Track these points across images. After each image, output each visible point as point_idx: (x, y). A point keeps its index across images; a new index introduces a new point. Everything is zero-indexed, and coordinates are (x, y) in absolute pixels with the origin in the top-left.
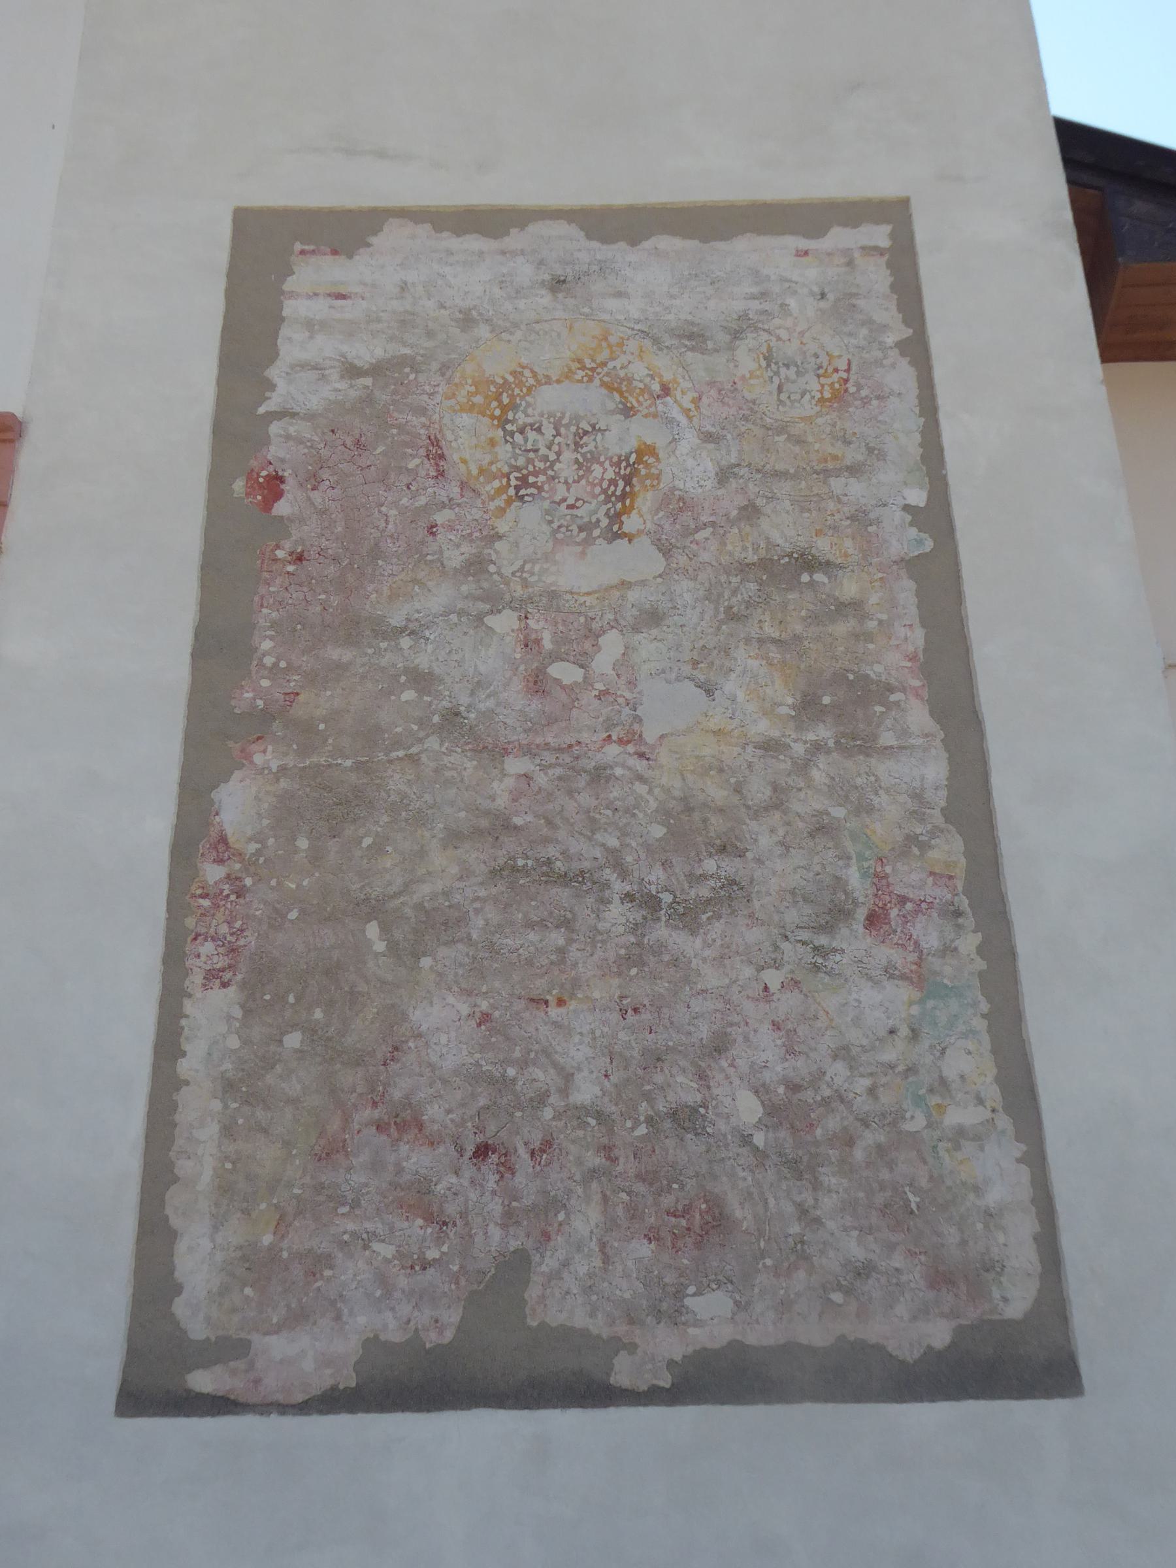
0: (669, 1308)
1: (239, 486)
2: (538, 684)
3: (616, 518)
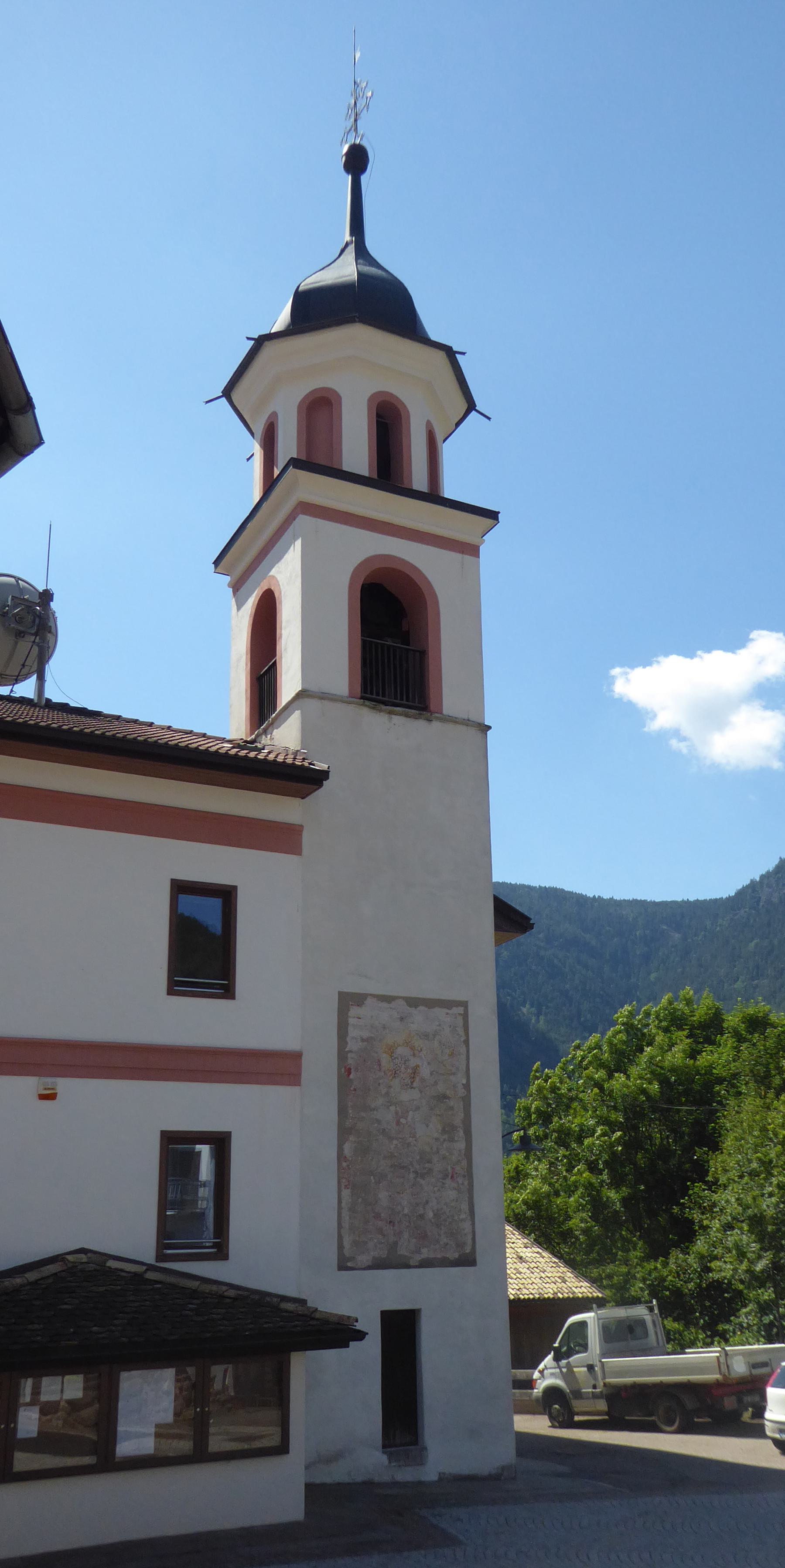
0: (418, 1252)
1: (343, 1070)
2: (398, 1123)
3: (412, 1083)
